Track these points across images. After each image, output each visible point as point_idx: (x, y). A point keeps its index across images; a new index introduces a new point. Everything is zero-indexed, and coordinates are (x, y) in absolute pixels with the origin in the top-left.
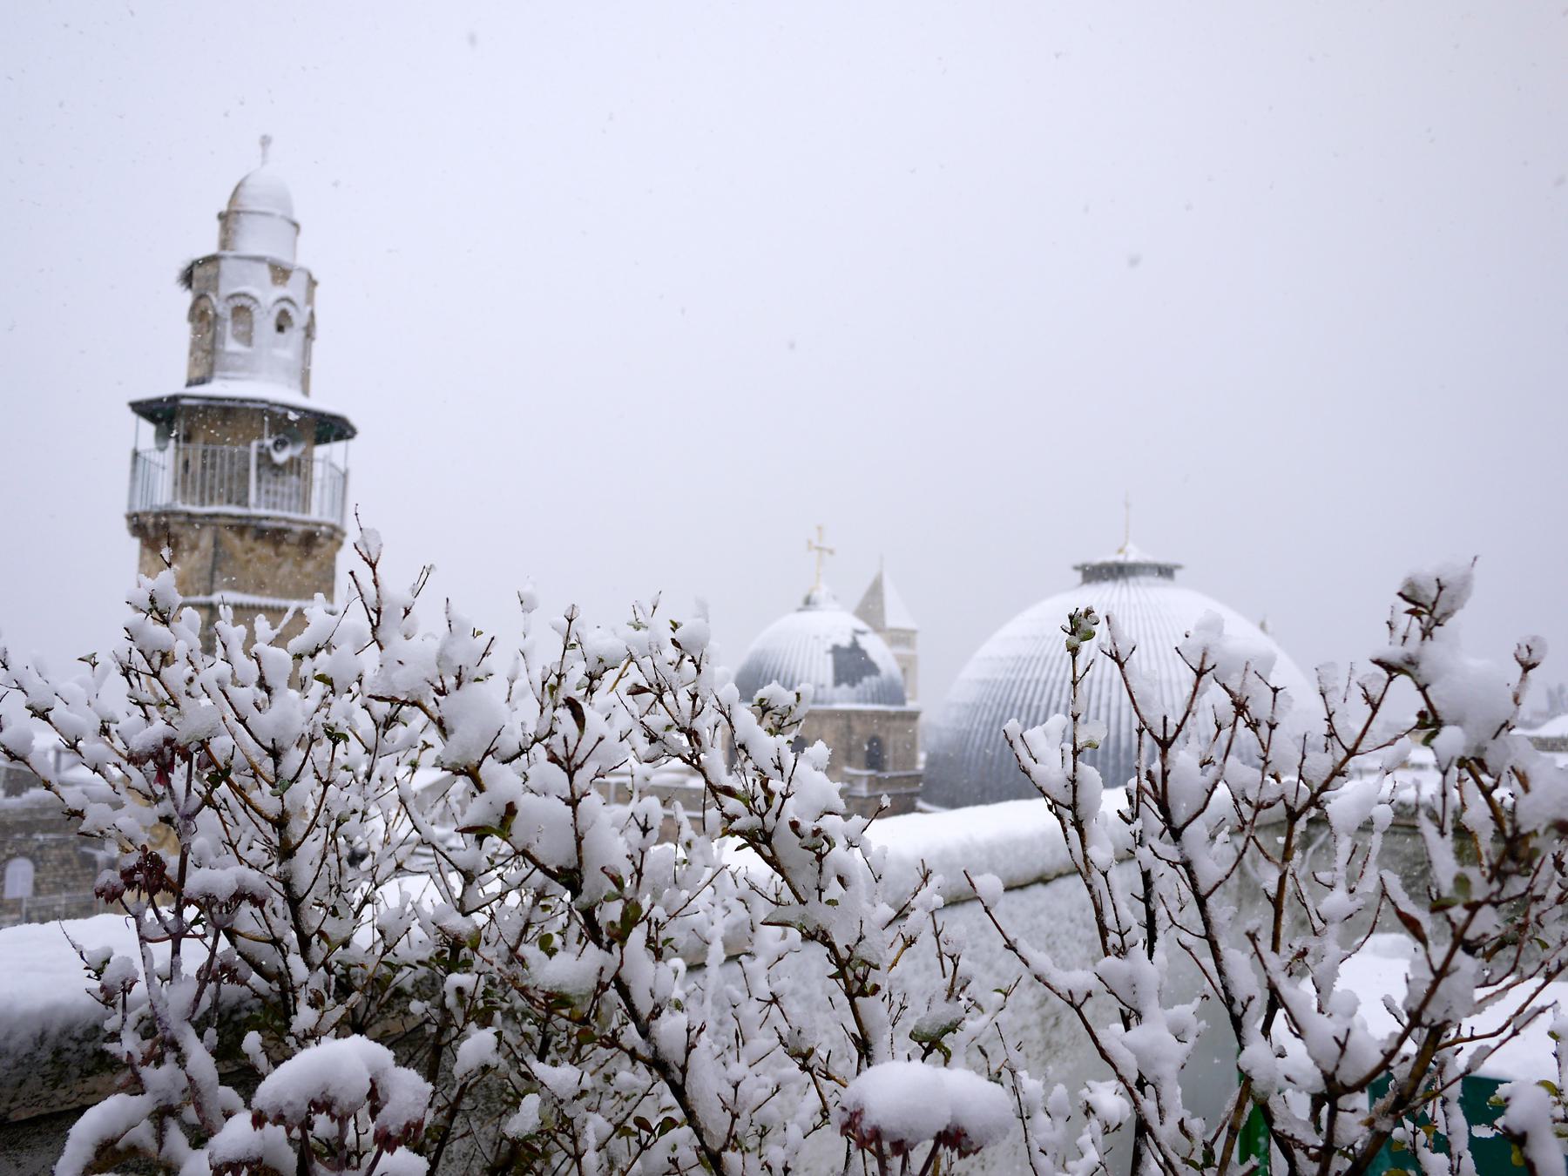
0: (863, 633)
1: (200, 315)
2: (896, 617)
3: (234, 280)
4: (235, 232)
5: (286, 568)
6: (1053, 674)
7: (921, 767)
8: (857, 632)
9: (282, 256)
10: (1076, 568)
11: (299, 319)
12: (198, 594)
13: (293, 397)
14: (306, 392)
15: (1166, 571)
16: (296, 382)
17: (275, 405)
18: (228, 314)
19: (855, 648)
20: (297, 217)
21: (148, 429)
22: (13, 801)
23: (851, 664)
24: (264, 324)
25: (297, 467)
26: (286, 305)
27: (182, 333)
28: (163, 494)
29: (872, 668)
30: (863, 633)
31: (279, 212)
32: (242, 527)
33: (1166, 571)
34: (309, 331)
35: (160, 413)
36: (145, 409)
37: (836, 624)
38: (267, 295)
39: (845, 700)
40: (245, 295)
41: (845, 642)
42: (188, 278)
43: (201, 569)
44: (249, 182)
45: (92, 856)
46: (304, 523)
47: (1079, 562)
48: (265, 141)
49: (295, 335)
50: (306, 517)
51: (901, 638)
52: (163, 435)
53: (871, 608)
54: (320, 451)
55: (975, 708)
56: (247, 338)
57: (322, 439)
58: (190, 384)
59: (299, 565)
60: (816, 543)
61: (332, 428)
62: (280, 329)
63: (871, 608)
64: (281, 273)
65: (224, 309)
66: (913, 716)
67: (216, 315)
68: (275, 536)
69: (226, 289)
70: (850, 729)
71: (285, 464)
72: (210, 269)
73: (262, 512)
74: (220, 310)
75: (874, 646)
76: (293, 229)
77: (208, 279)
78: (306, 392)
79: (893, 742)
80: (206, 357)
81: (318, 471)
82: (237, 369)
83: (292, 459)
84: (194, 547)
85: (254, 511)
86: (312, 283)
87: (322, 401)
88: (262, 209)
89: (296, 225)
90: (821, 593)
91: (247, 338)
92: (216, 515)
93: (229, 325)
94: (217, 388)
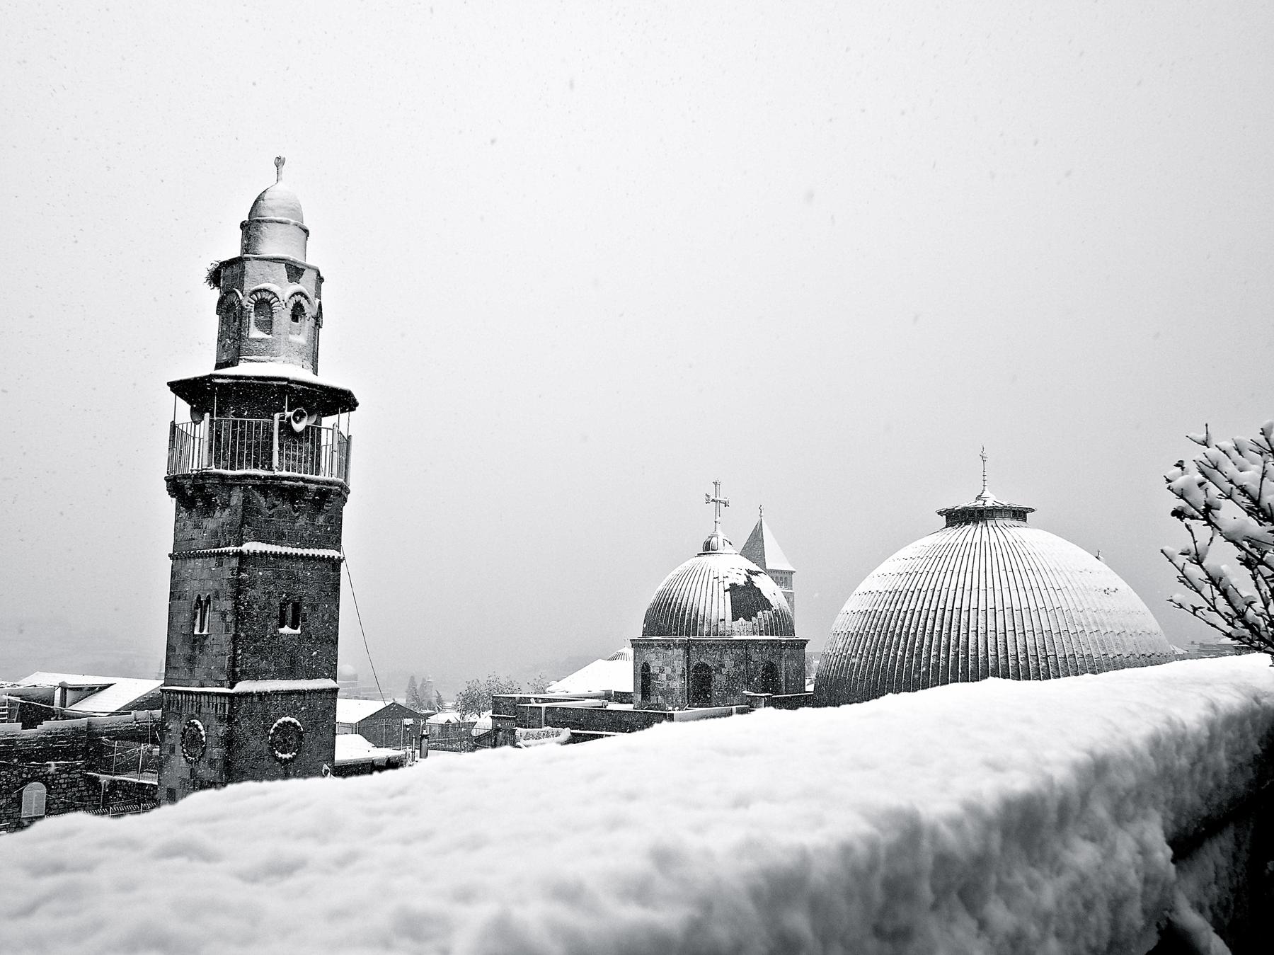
0: (756, 573)
1: (228, 309)
2: (775, 560)
3: (259, 278)
4: (257, 239)
5: (302, 521)
6: (926, 606)
7: (810, 688)
8: (750, 572)
9: (294, 255)
10: (940, 513)
11: (310, 311)
12: (228, 545)
13: (306, 375)
14: (315, 372)
15: (1020, 514)
16: (308, 364)
17: (293, 382)
18: (251, 307)
19: (750, 584)
20: (306, 225)
21: (184, 408)
22: (29, 733)
23: (746, 600)
24: (282, 316)
25: (313, 434)
26: (298, 298)
27: (213, 322)
28: (198, 460)
29: (766, 605)
30: (756, 573)
31: (293, 221)
32: (269, 487)
33: (1020, 514)
34: (318, 319)
35: (192, 391)
36: (182, 388)
37: (731, 566)
38: (284, 289)
39: (741, 631)
40: (265, 290)
41: (741, 581)
42: (215, 278)
43: (231, 524)
44: (266, 196)
45: (98, 778)
46: (317, 482)
47: (944, 507)
48: (279, 162)
49: (307, 324)
50: (321, 477)
51: (782, 578)
52: (197, 413)
53: (754, 548)
54: (327, 421)
55: (858, 636)
56: (267, 326)
57: (331, 411)
58: (218, 366)
59: (312, 518)
60: (713, 497)
61: (341, 401)
62: (295, 318)
63: (754, 548)
64: (295, 271)
65: (248, 303)
66: (803, 644)
67: (242, 307)
68: (292, 493)
69: (249, 286)
70: (748, 658)
71: (301, 433)
72: (236, 270)
73: (285, 473)
74: (244, 303)
75: (765, 585)
76: (304, 235)
77: (234, 277)
78: (315, 372)
79: (785, 667)
80: (233, 344)
81: (326, 438)
82: (260, 353)
83: (307, 427)
84: (225, 506)
85: (277, 473)
86: (320, 280)
87: (328, 377)
88: (278, 218)
89: (306, 231)
90: (717, 542)
91: (267, 326)
92: (246, 477)
93: (252, 315)
94: (244, 369)
